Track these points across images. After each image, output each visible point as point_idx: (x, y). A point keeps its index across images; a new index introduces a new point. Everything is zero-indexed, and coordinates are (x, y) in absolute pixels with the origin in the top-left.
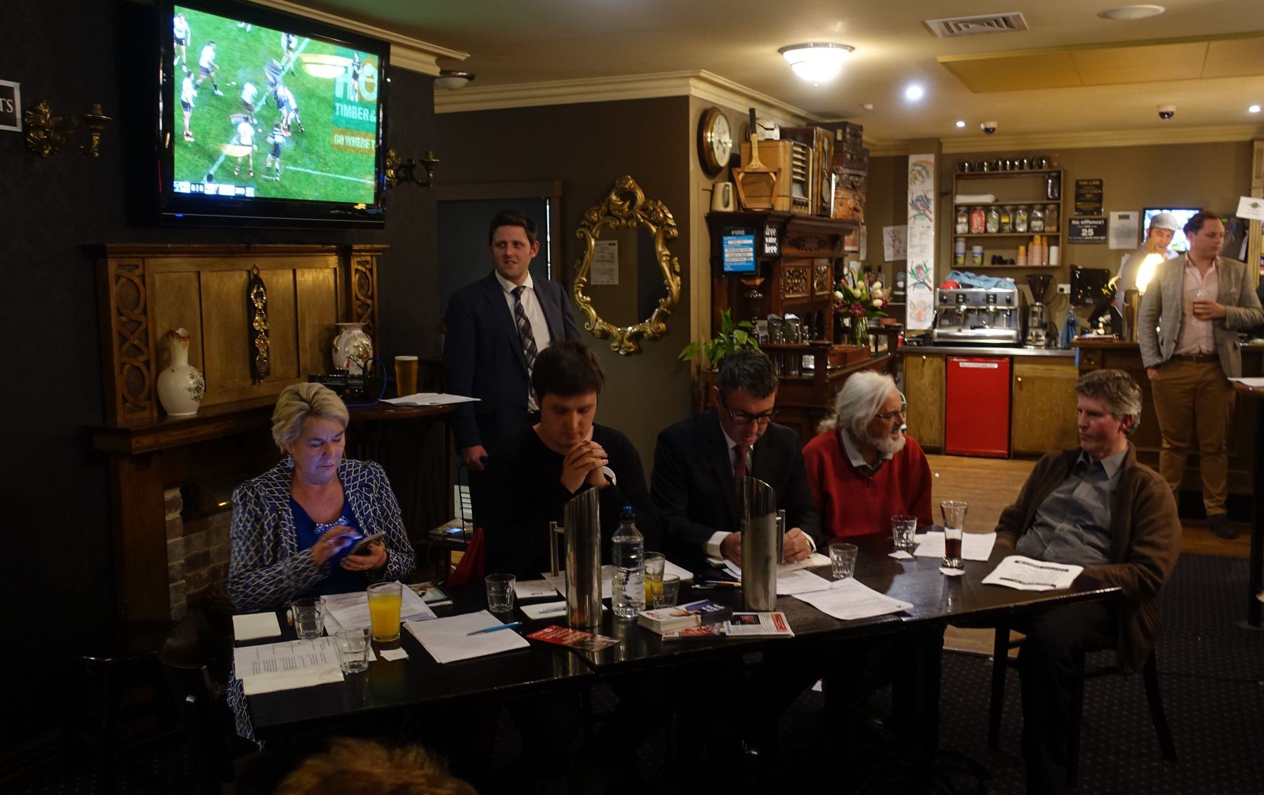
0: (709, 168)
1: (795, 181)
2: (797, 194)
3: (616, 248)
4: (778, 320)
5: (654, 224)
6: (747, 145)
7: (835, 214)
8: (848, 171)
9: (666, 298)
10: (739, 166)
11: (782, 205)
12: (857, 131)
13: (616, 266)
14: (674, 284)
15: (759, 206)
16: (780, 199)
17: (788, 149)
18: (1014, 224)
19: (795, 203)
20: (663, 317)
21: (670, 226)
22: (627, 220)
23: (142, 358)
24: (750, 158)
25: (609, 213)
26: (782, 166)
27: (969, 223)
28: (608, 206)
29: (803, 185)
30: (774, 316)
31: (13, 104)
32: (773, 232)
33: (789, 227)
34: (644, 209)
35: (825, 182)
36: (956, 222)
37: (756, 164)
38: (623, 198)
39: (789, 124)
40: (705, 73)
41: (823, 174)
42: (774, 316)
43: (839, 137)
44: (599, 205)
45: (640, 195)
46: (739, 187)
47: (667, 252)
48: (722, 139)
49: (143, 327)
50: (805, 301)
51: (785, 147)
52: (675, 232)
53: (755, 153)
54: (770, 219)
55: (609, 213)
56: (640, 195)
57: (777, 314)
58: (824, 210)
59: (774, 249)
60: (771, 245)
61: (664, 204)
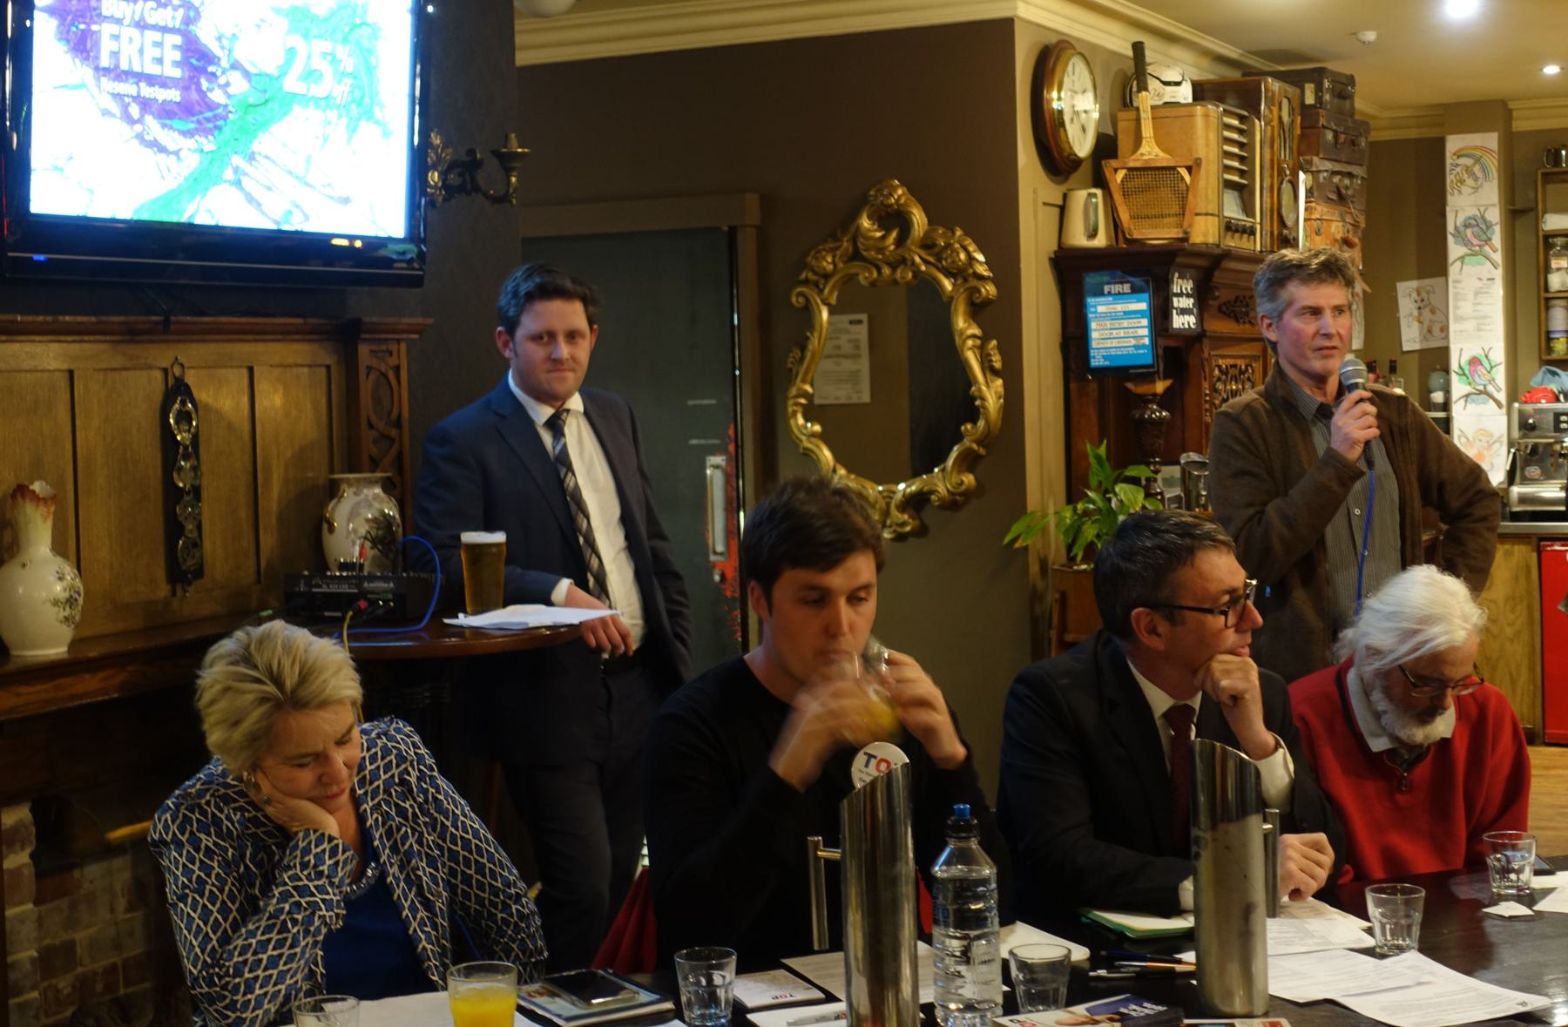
1: (1229, 185)
2: (1233, 210)
3: (862, 332)
5: (948, 274)
6: (1132, 115)
8: (1329, 165)
9: (974, 422)
11: (1204, 232)
12: (1344, 88)
13: (864, 365)
14: (991, 394)
15: (1158, 234)
17: (1213, 121)
19: (1230, 227)
20: (969, 461)
21: (981, 278)
22: (894, 268)
24: (1138, 140)
25: (856, 256)
26: (1201, 153)
28: (854, 240)
29: (1244, 192)
30: (1194, 456)
32: (1188, 286)
33: (1218, 277)
34: (927, 245)
35: (1286, 187)
36: (1547, 269)
37: (1150, 152)
39: (1209, 73)
41: (1281, 172)
42: (1194, 456)
44: (836, 239)
45: (919, 218)
46: (1118, 197)
47: (976, 331)
48: (1079, 105)
51: (1206, 116)
53: (1147, 130)
54: (1179, 260)
55: (856, 256)
56: (919, 218)
60: (1184, 312)
61: (967, 234)
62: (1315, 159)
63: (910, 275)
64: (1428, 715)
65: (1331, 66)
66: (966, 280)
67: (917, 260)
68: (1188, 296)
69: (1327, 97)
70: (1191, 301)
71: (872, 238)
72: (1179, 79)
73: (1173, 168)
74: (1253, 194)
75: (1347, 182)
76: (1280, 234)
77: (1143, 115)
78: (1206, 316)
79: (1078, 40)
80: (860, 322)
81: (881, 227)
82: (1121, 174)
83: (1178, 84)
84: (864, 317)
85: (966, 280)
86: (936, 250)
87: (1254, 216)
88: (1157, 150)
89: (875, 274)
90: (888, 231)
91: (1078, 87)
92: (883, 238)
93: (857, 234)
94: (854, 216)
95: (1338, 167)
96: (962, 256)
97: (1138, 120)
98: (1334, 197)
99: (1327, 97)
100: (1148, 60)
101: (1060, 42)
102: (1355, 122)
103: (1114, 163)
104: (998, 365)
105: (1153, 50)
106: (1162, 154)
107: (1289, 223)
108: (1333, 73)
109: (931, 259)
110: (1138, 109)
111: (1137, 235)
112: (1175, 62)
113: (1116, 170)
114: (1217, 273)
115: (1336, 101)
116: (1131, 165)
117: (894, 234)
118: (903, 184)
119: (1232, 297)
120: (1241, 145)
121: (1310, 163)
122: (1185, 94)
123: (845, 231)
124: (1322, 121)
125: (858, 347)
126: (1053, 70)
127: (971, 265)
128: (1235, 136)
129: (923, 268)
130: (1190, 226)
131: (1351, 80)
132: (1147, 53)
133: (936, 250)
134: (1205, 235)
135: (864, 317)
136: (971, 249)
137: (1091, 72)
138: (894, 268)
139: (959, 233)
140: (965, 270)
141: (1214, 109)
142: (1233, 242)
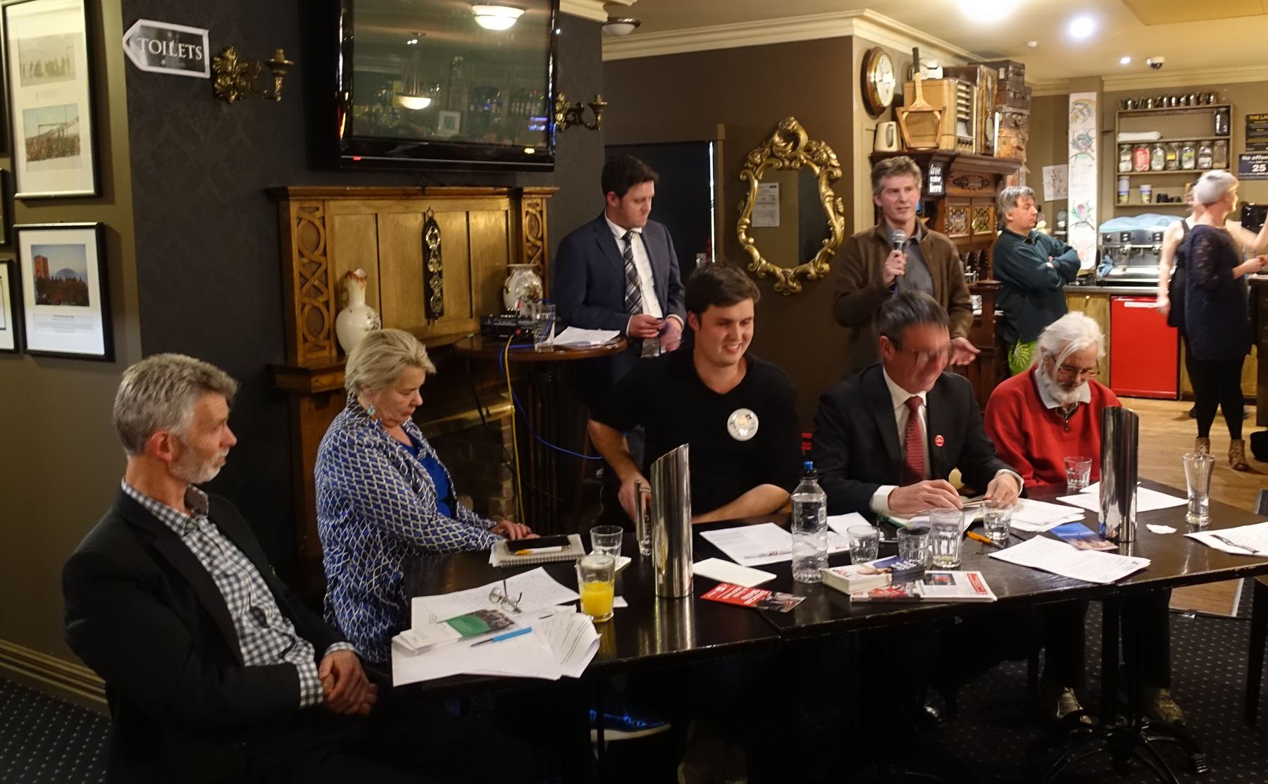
0: (873, 109)
2: (961, 132)
3: (777, 190)
5: (818, 164)
8: (1011, 109)
9: (830, 238)
11: (947, 144)
12: (1019, 71)
15: (924, 145)
17: (953, 87)
18: (1180, 161)
19: (960, 141)
20: (827, 258)
23: (322, 299)
25: (772, 155)
27: (1133, 160)
29: (967, 123)
31: (202, 51)
32: (938, 171)
33: (953, 166)
34: (808, 149)
35: (989, 120)
37: (920, 103)
39: (951, 63)
40: (869, 13)
41: (987, 113)
45: (803, 137)
48: (885, 82)
49: (323, 268)
52: (838, 173)
53: (919, 92)
55: (772, 155)
58: (988, 150)
60: (935, 184)
64: (1069, 386)
82: (905, 114)
94: (772, 135)
103: (902, 109)
104: (841, 210)
111: (913, 145)
122: (938, 74)
141: (953, 82)
142: (961, 149)
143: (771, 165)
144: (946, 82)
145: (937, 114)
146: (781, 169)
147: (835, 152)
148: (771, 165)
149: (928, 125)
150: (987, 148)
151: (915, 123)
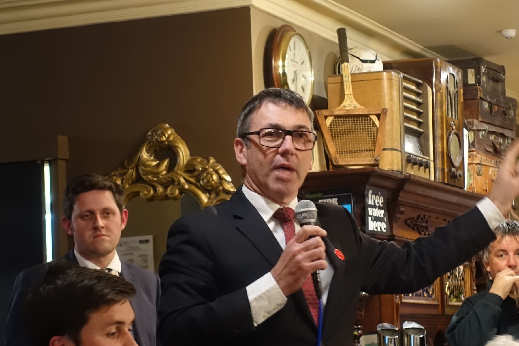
1: (408, 131)
2: (410, 146)
3: (150, 247)
4: (392, 332)
5: (205, 190)
6: (337, 79)
7: (471, 187)
8: (486, 127)
10: (326, 107)
11: (390, 163)
12: (497, 74)
15: (357, 162)
16: (387, 154)
17: (395, 83)
19: (410, 160)
22: (166, 188)
24: (342, 97)
25: (139, 179)
26: (387, 105)
29: (420, 136)
30: (387, 325)
32: (380, 201)
33: (402, 197)
34: (190, 169)
35: (453, 138)
37: (351, 104)
38: (160, 158)
39: (396, 56)
41: (449, 127)
42: (387, 325)
43: (471, 80)
44: (124, 167)
45: (184, 153)
46: (327, 136)
48: (298, 70)
50: (433, 312)
51: (390, 79)
53: (348, 89)
54: (372, 180)
55: (139, 179)
57: (392, 322)
58: (454, 177)
59: (382, 226)
60: (377, 219)
61: (218, 161)
62: (476, 122)
63: (177, 192)
65: (486, 58)
66: (217, 195)
67: (182, 180)
68: (380, 208)
69: (484, 79)
70: (383, 212)
71: (149, 166)
72: (373, 58)
73: (367, 116)
74: (427, 139)
75: (501, 140)
76: (450, 171)
77: (345, 79)
78: (395, 225)
79: (299, 27)
80: (147, 241)
81: (157, 158)
82: (330, 120)
83: (373, 62)
84: (150, 237)
85: (217, 195)
86: (196, 173)
87: (428, 155)
88: (355, 103)
89: (152, 192)
90: (162, 161)
91: (298, 59)
92: (158, 165)
93: (140, 163)
94: (137, 150)
95: (493, 129)
96: (215, 177)
97: (342, 83)
98: (491, 150)
99: (484, 79)
100: (349, 46)
101: (283, 27)
102: (505, 98)
103: (324, 112)
105: (353, 39)
106: (359, 106)
107: (457, 164)
108: (488, 62)
109: (192, 180)
110: (342, 76)
111: (341, 162)
112: (367, 48)
113: (326, 117)
114: (401, 194)
115: (491, 83)
116: (337, 113)
117: (166, 163)
118: (172, 126)
119: (415, 215)
120: (418, 104)
121: (472, 124)
122: (378, 66)
123: (130, 162)
124: (480, 95)
125: (146, 261)
126: (279, 44)
127: (221, 184)
128: (414, 97)
129: (187, 186)
130: (379, 156)
131: (503, 69)
132: (349, 41)
133: (196, 173)
134: (392, 164)
135: (150, 237)
136: (221, 172)
137: (307, 48)
138: (166, 188)
139: (212, 161)
140: (217, 188)
141: (396, 76)
142: (412, 171)
143: (137, 194)
144: (385, 73)
145: (374, 118)
146: (151, 199)
147: (229, 173)
148: (137, 194)
149: (363, 135)
150: (454, 176)
151: (346, 132)
